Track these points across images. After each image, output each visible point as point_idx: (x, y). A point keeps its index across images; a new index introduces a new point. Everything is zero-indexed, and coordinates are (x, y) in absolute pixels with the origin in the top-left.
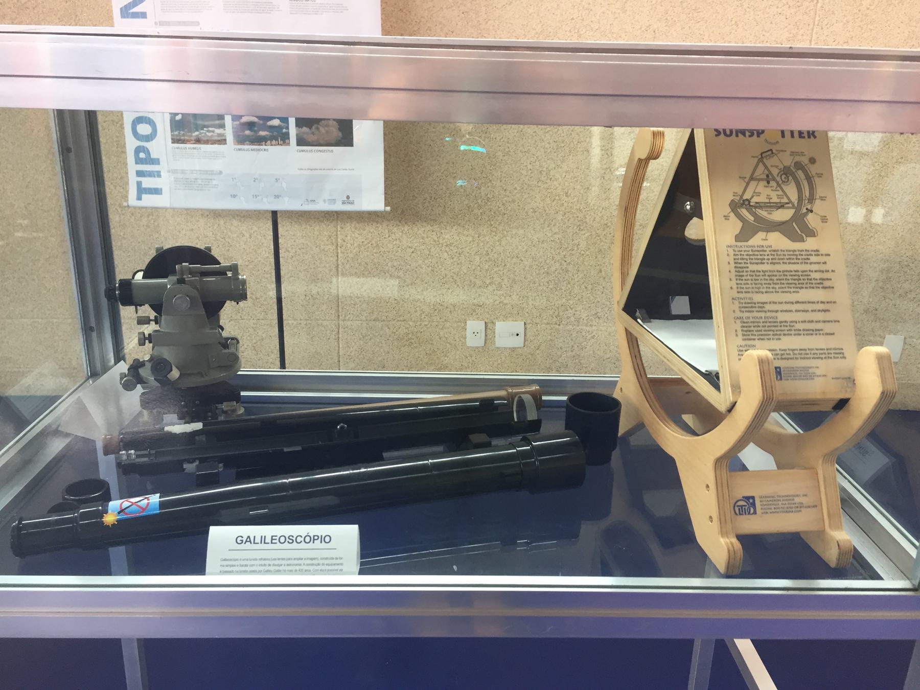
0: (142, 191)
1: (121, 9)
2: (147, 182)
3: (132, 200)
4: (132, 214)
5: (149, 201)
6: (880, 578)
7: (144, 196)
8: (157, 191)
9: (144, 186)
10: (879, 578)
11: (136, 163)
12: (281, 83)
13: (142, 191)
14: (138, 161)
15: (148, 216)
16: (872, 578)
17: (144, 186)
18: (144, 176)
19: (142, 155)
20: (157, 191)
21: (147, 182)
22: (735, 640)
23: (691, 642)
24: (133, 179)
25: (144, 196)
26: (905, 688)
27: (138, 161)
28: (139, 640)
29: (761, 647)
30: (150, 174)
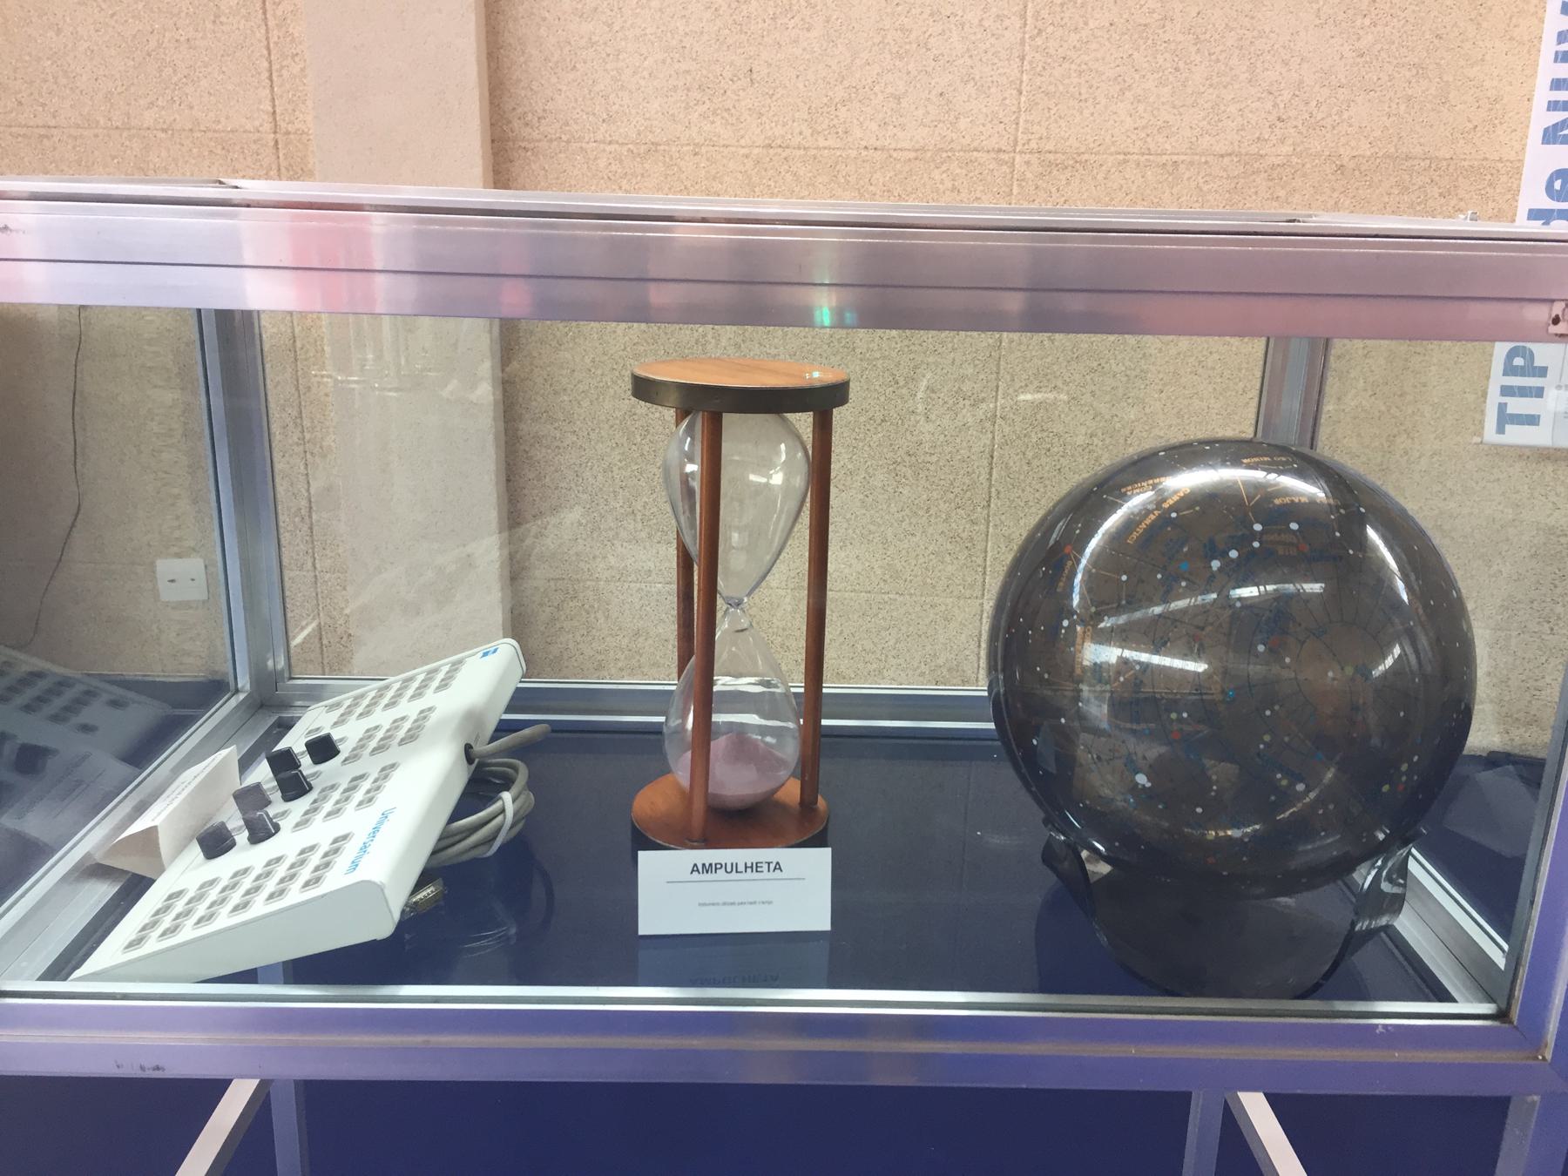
0: (1505, 419)
1: (1546, 130)
2: (1516, 405)
3: (1490, 434)
4: (1406, 453)
5: (1517, 435)
6: (1454, 1000)
7: (1508, 427)
8: (1532, 420)
9: (1509, 411)
10: (1452, 1000)
11: (1505, 374)
12: (344, 274)
13: (1504, 419)
14: (1510, 370)
15: (1432, 456)
16: (1441, 1000)
17: (1509, 411)
18: (1513, 395)
19: (1518, 361)
20: (1532, 420)
21: (1516, 405)
22: (1241, 1095)
23: (1186, 1097)
24: (1494, 398)
25: (1508, 427)
26: (1498, 1171)
27: (1510, 370)
28: (297, 1083)
29: (1275, 1101)
30: (1523, 392)
